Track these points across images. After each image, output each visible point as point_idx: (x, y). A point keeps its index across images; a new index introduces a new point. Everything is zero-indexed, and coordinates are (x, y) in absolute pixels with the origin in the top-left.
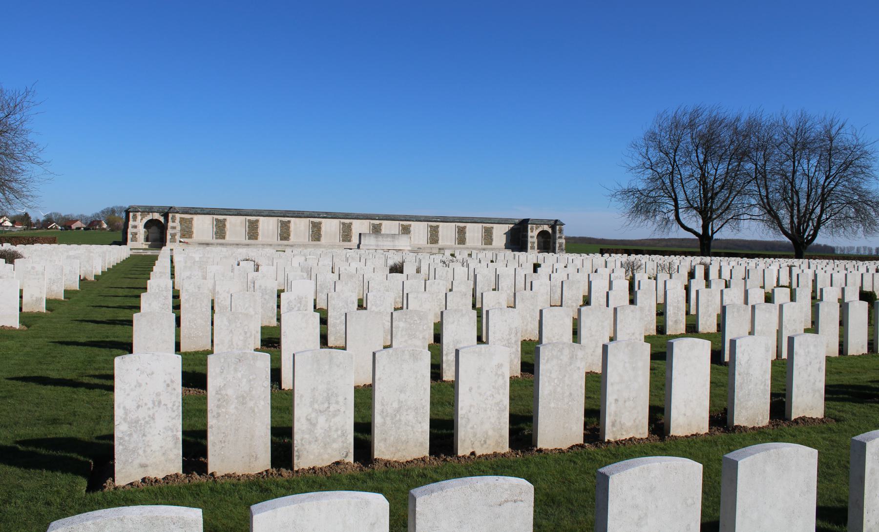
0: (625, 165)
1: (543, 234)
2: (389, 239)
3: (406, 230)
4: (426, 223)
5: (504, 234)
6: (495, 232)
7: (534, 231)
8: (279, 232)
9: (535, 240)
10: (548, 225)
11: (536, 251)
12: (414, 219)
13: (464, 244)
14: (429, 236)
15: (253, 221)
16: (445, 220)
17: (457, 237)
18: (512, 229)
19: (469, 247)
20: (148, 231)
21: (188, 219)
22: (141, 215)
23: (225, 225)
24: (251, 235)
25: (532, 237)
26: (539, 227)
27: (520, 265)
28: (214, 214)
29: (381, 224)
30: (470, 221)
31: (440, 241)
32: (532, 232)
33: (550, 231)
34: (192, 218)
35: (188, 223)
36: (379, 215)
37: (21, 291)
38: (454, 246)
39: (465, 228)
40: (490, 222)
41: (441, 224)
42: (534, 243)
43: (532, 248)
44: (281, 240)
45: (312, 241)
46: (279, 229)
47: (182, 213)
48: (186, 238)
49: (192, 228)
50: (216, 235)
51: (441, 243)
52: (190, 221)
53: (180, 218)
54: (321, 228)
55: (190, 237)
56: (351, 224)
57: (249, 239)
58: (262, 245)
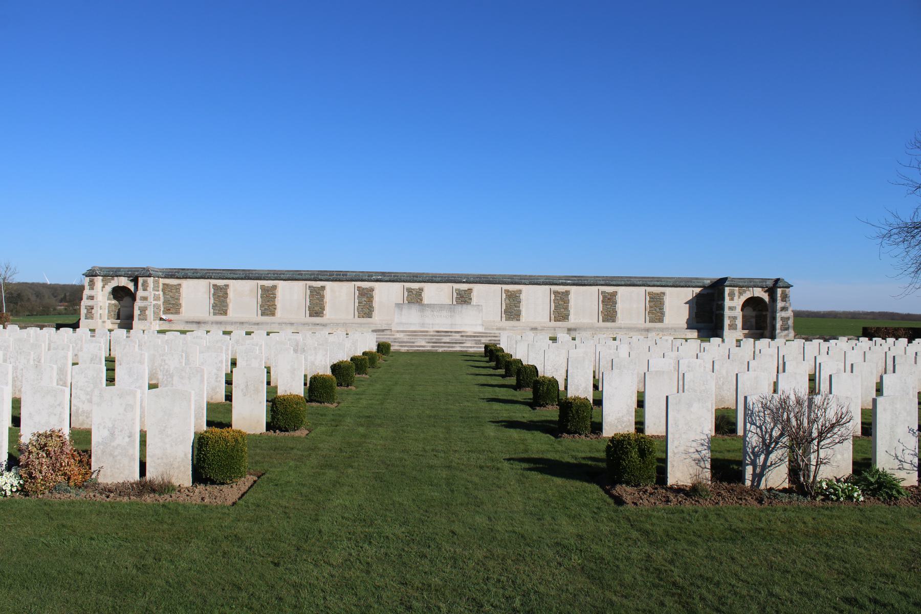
0: (906, 182)
1: (752, 303)
2: (444, 313)
3: (464, 299)
4: (547, 287)
5: (686, 303)
6: (667, 301)
7: (736, 298)
8: (308, 304)
9: (738, 313)
10: (762, 287)
11: (739, 333)
12: (527, 281)
13: (614, 321)
14: (553, 308)
15: (268, 287)
16: (580, 282)
17: (601, 309)
18: (698, 296)
19: (623, 326)
20: (120, 304)
21: (175, 285)
22: (102, 280)
23: (227, 294)
24: (265, 309)
25: (731, 308)
26: (745, 292)
27: (848, 368)
28: (211, 278)
29: (470, 290)
30: (623, 283)
31: (571, 317)
32: (732, 299)
33: (766, 297)
34: (180, 285)
35: (175, 291)
36: (468, 275)
37: (16, 404)
38: (598, 325)
39: (614, 294)
40: (658, 283)
41: (573, 289)
42: (735, 318)
43: (733, 327)
44: (310, 316)
45: (359, 317)
46: (308, 300)
47: (165, 277)
48: (172, 313)
49: (179, 299)
50: (214, 310)
51: (573, 320)
52: (177, 289)
53: (164, 284)
54: (372, 297)
55: (177, 312)
56: (421, 290)
57: (262, 315)
58: (240, 323)
